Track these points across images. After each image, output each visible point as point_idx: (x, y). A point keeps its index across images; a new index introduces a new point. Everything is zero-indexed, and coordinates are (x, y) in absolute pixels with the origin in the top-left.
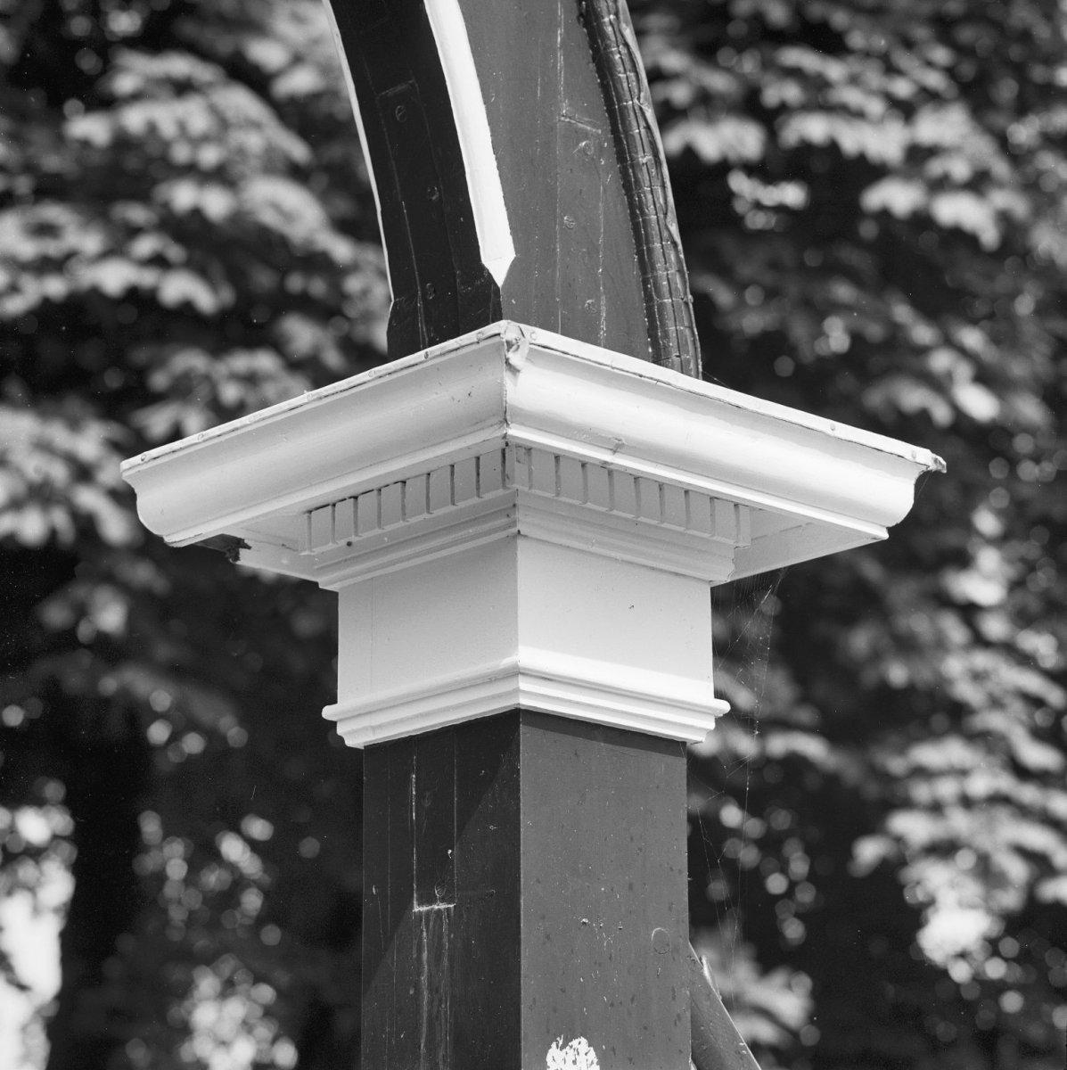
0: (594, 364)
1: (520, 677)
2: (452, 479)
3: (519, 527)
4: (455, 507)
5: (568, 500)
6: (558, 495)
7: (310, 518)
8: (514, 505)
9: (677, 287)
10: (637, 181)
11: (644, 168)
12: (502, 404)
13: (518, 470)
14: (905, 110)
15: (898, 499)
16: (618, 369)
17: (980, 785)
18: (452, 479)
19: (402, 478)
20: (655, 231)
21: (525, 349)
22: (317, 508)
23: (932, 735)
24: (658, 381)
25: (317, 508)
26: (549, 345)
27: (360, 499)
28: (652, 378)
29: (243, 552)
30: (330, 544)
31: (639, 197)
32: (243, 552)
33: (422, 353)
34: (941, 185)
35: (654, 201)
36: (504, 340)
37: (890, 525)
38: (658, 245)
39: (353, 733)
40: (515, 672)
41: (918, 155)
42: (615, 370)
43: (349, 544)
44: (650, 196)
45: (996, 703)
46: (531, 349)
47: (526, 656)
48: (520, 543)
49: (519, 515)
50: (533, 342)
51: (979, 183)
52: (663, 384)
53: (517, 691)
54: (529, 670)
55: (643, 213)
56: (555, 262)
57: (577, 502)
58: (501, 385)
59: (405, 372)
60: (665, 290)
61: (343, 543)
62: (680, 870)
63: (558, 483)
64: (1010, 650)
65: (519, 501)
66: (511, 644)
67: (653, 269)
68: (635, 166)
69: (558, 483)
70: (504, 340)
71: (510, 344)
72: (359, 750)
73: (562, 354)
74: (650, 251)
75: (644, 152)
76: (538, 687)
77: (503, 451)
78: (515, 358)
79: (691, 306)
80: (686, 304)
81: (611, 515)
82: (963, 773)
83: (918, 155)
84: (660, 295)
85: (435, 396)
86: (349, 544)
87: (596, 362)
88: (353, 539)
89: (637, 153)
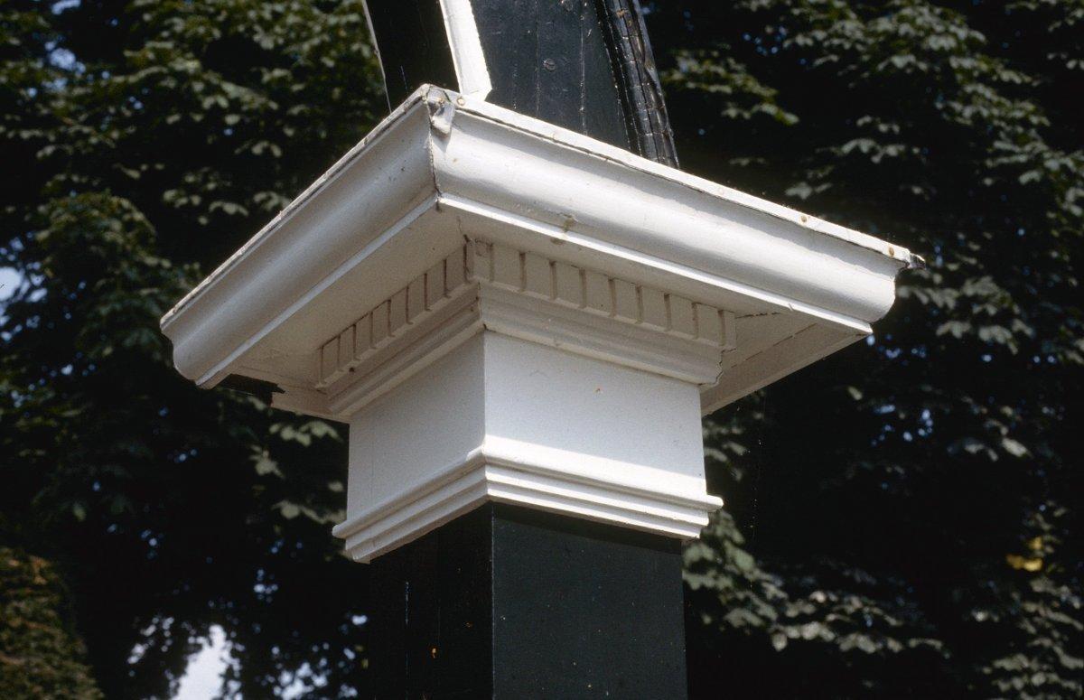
0: (532, 135)
1: (487, 468)
2: (425, 284)
3: (484, 320)
4: (429, 313)
5: (535, 295)
6: (524, 288)
7: (322, 352)
8: (477, 298)
9: (657, 123)
10: (616, 32)
11: (622, 21)
12: (430, 171)
13: (479, 263)
14: (953, 281)
15: (881, 291)
16: (561, 143)
17: (1038, 680)
18: (425, 284)
19: (386, 298)
20: (634, 74)
21: (450, 113)
22: (327, 343)
23: (1008, 653)
24: (608, 158)
25: (327, 343)
26: (479, 111)
27: (357, 325)
28: (600, 155)
29: (275, 396)
30: (337, 372)
31: (619, 47)
32: (275, 396)
33: (363, 141)
34: (984, 319)
35: (632, 49)
36: (426, 102)
37: (873, 321)
38: (637, 87)
39: (356, 548)
40: (483, 462)
41: (965, 304)
42: (558, 144)
43: (352, 370)
44: (628, 45)
45: (1044, 632)
46: (456, 114)
47: (493, 445)
48: (489, 343)
49: (482, 307)
50: (460, 107)
51: (1004, 319)
52: (613, 162)
53: (485, 483)
54: (495, 459)
55: (623, 61)
56: (535, 98)
57: (546, 298)
58: (427, 157)
59: (352, 163)
60: (646, 125)
61: (346, 369)
62: (677, 667)
63: (523, 278)
64: (1046, 599)
65: (481, 294)
66: (477, 434)
67: (635, 109)
68: (613, 18)
69: (523, 278)
70: (426, 102)
71: (433, 107)
72: (366, 565)
73: (495, 123)
74: (631, 93)
75: (621, 7)
76: (518, 480)
77: (465, 249)
78: (440, 122)
79: (671, 139)
80: (667, 137)
81: (583, 312)
82: (1030, 673)
83: (965, 304)
84: (642, 132)
85: (376, 182)
86: (352, 370)
87: (536, 134)
88: (353, 364)
89: (613, 8)
